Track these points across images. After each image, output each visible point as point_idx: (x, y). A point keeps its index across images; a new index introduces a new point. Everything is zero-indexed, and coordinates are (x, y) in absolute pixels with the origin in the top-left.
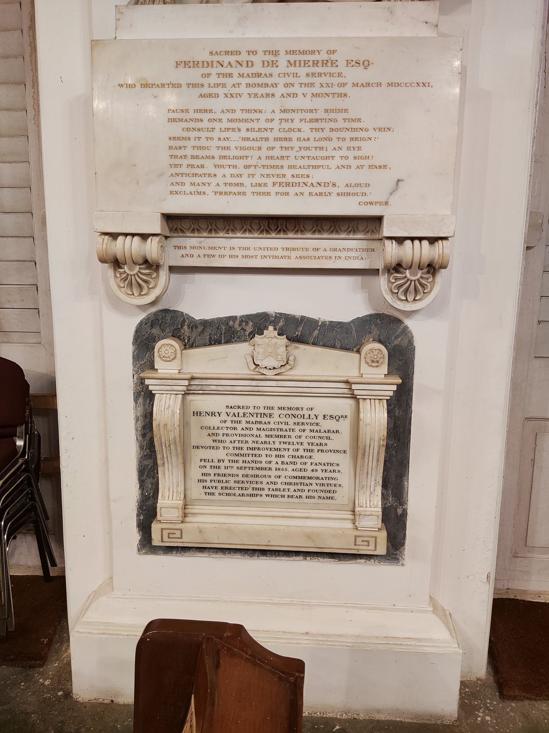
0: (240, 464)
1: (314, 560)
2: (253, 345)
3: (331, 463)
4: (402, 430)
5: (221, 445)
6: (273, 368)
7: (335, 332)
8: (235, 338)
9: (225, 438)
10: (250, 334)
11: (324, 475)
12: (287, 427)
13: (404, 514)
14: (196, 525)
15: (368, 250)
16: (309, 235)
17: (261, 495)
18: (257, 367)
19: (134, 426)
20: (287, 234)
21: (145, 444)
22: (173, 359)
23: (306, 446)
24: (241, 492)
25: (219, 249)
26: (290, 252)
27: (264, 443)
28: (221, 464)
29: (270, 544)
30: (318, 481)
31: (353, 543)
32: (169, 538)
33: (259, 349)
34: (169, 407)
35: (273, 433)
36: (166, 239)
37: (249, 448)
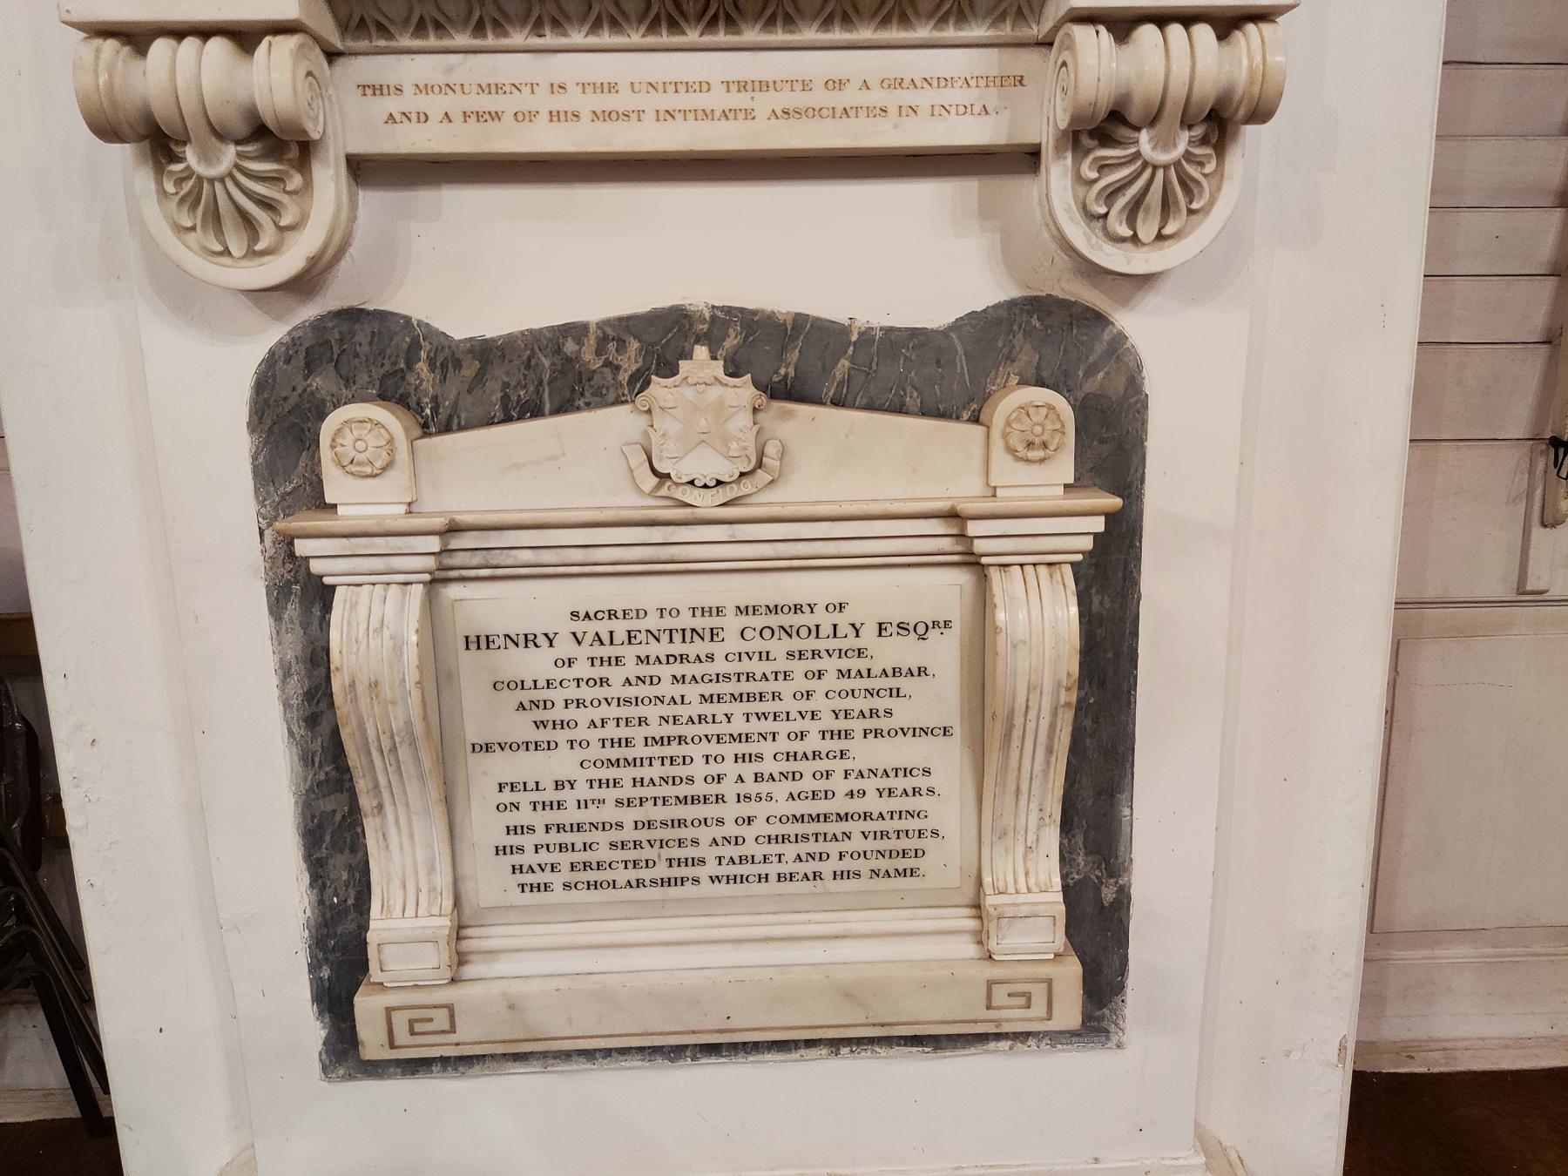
0: (627, 791)
1: (863, 1054)
2: (645, 412)
3: (905, 769)
4: (1110, 655)
5: (561, 736)
6: (714, 483)
7: (902, 361)
8: (587, 394)
9: (572, 713)
10: (633, 379)
11: (886, 805)
12: (768, 667)
13: (1123, 901)
14: (496, 988)
15: (1002, 81)
16: (810, 34)
17: (696, 881)
18: (665, 482)
19: (276, 692)
20: (738, 33)
21: (317, 746)
22: (384, 469)
23: (828, 722)
24: (632, 874)
25: (514, 90)
26: (753, 94)
27: (696, 720)
28: (566, 795)
29: (730, 1025)
30: (869, 826)
31: (984, 1003)
32: (413, 1033)
33: (668, 424)
34: (382, 627)
35: (724, 688)
36: (330, 62)
37: (649, 740)
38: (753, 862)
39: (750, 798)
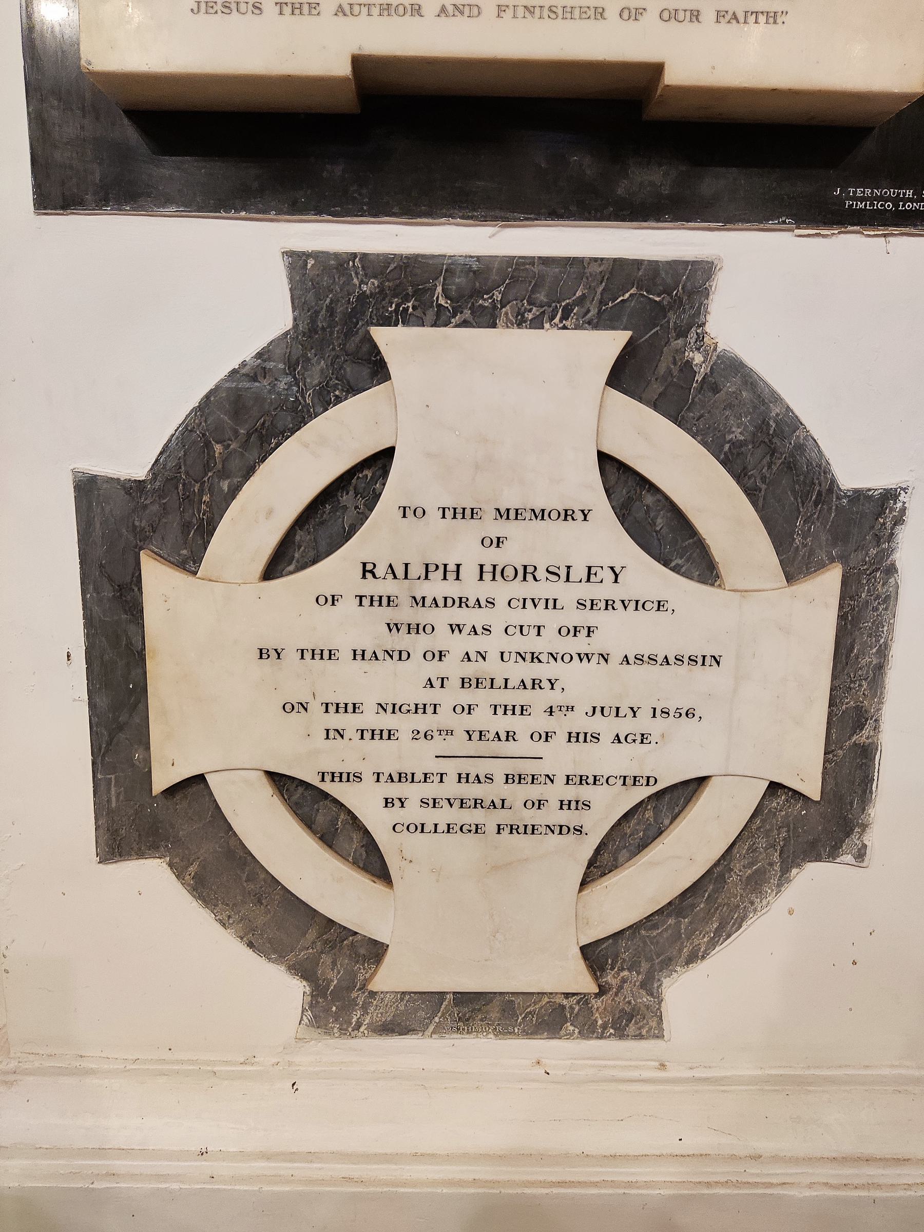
38: (413, 781)
39: (668, 713)
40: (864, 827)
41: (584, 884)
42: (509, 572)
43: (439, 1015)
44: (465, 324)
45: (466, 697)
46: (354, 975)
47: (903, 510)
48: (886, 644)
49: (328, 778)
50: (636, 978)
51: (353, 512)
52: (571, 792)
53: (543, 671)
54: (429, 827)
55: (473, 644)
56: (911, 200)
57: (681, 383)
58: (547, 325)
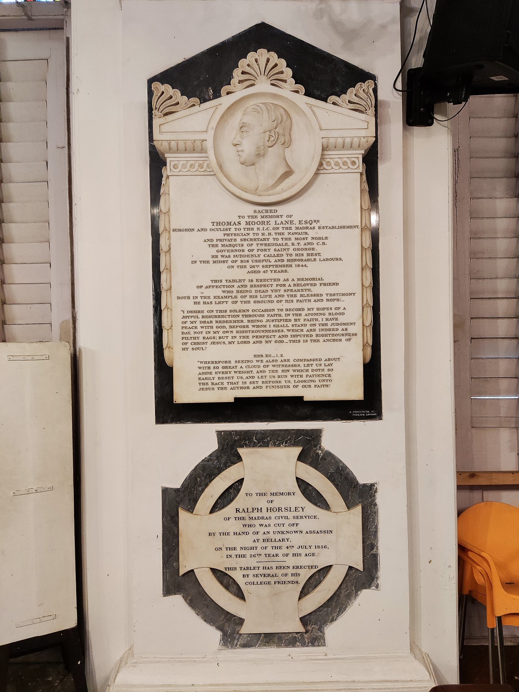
40: (377, 578)
41: (300, 599)
42: (275, 509)
43: (260, 641)
44: (261, 446)
45: (265, 544)
46: (235, 629)
47: (376, 489)
48: (377, 524)
49: (227, 569)
50: (317, 627)
51: (233, 494)
52: (295, 571)
53: (285, 536)
54: (256, 583)
55: (266, 529)
56: (369, 413)
57: (316, 458)
58: (281, 445)
